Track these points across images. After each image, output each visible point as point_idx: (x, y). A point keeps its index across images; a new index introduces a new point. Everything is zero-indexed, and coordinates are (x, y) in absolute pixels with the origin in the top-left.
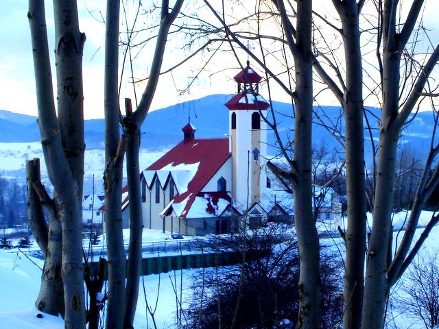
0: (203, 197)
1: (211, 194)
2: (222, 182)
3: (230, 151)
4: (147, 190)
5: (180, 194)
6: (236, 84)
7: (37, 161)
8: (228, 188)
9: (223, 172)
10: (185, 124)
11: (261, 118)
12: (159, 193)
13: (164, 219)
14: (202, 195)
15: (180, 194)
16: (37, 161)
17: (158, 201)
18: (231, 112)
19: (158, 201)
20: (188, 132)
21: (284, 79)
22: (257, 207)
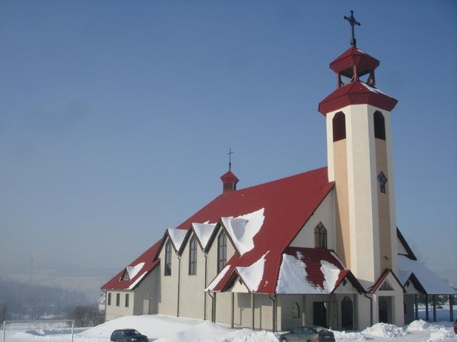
0: (295, 255)
1: (305, 251)
2: (321, 232)
3: (331, 178)
4: (174, 255)
5: (242, 253)
6: (337, 75)
7: (165, 275)
8: (330, 245)
9: (322, 215)
10: (225, 171)
11: (198, 247)
12: (195, 254)
13: (214, 299)
14: (291, 251)
15: (242, 253)
16: (165, 275)
17: (192, 271)
18: (331, 116)
19: (192, 271)
20: (229, 180)
21: (198, 247)
22: (389, 278)
